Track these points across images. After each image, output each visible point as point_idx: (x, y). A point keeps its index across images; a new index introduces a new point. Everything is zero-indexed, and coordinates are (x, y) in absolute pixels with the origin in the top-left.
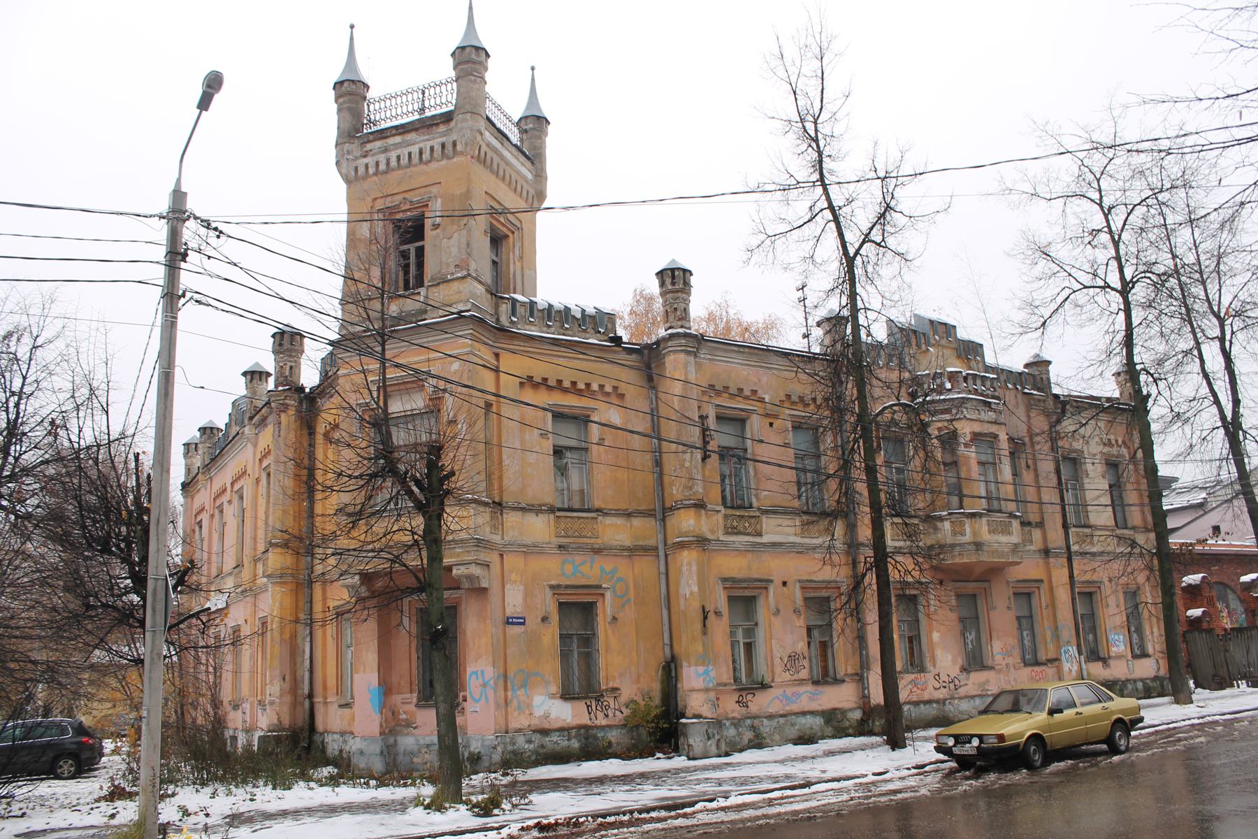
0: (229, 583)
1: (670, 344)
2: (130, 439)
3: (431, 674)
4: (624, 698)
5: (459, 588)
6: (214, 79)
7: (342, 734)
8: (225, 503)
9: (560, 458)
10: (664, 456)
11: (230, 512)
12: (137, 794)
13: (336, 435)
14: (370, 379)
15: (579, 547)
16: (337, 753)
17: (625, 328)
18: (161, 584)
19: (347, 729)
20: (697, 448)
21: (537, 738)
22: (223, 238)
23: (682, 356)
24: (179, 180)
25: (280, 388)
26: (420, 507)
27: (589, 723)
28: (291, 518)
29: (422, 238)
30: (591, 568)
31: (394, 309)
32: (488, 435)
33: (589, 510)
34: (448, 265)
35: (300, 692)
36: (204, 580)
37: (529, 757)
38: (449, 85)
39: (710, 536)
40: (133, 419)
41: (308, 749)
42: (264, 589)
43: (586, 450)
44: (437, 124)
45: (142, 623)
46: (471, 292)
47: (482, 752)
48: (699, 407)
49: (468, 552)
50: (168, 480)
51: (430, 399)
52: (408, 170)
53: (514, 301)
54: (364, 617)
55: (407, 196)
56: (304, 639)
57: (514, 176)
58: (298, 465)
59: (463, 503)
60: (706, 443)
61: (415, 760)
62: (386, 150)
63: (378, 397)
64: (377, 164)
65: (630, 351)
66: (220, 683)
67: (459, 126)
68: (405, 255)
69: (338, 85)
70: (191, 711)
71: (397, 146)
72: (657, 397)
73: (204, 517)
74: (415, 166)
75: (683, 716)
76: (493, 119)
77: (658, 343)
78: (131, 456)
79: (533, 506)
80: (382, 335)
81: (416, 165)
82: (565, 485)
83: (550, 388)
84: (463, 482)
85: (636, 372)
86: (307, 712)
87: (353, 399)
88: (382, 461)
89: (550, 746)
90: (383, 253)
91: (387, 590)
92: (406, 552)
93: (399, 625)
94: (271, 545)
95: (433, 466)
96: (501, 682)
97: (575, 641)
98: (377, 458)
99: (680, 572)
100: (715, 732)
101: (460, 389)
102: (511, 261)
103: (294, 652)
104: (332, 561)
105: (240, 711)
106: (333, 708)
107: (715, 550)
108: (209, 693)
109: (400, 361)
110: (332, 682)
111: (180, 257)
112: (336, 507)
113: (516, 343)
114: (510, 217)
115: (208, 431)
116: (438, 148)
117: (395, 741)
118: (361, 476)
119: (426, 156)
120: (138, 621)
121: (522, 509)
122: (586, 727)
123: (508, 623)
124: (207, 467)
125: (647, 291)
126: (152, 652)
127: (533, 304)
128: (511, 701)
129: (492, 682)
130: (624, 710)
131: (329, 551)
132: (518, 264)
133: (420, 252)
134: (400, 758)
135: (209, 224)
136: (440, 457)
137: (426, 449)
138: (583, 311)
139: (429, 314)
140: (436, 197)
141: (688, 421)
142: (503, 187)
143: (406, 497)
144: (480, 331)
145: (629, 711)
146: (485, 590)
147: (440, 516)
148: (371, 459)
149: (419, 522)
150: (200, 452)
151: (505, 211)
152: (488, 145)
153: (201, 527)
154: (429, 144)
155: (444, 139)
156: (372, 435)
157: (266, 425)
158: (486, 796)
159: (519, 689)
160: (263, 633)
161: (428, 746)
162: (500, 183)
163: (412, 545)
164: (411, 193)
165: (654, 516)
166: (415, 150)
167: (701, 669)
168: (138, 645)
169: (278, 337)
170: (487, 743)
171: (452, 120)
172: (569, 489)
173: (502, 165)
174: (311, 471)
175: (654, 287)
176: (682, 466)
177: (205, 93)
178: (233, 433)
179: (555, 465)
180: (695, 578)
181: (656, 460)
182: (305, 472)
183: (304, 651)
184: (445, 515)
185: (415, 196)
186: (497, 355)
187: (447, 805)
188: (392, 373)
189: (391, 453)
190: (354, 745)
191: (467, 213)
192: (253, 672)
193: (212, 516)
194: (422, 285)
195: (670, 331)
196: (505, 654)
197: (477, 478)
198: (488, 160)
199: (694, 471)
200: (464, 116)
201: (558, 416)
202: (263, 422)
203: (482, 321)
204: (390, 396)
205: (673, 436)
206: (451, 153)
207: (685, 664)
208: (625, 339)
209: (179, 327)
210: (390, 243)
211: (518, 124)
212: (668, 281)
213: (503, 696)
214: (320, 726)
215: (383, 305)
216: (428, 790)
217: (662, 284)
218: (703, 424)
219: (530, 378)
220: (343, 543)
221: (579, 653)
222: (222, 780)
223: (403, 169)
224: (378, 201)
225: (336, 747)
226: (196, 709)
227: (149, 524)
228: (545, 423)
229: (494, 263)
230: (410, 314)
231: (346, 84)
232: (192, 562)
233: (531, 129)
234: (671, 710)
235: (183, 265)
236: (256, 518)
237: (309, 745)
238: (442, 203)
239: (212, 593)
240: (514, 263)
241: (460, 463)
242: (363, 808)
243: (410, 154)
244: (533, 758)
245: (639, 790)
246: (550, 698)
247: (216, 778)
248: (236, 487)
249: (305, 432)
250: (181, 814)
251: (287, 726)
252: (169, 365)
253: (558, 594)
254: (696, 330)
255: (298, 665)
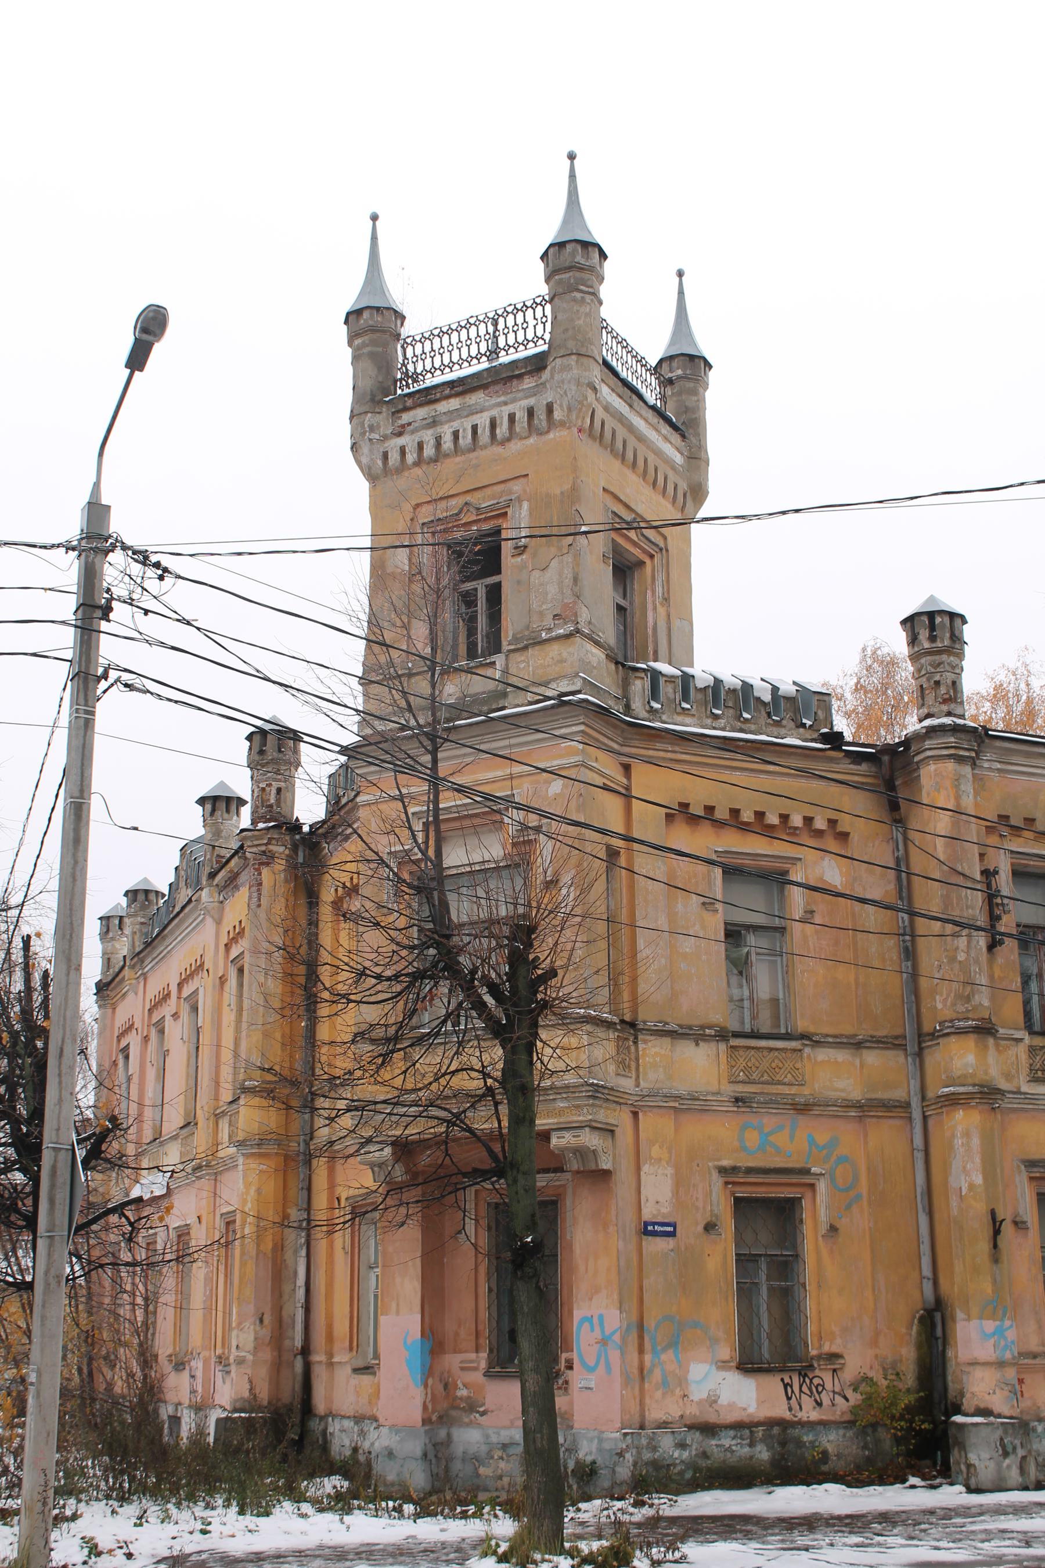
0: (172, 1156)
1: (928, 744)
2: (14, 913)
3: (513, 1319)
4: (849, 1374)
5: (559, 1170)
6: (154, 319)
7: (358, 1419)
8: (168, 1018)
9: (738, 946)
10: (921, 942)
11: (176, 1033)
12: (17, 1512)
13: (355, 905)
14: (411, 810)
15: (771, 1102)
16: (348, 1453)
17: (848, 715)
18: (64, 1158)
19: (366, 1410)
20: (979, 929)
21: (694, 1439)
22: (169, 580)
23: (950, 766)
24: (97, 486)
25: (261, 825)
26: (498, 1031)
27: (787, 1415)
28: (278, 1047)
29: (498, 571)
30: (792, 1137)
31: (451, 691)
32: (612, 907)
33: (787, 1037)
34: (541, 614)
35: (287, 1343)
36: (131, 1150)
37: (681, 1473)
38: (539, 309)
39: (1003, 1085)
40: (21, 878)
41: (299, 1444)
42: (230, 1165)
43: (782, 930)
44: (520, 377)
45: (31, 1222)
46: (581, 660)
47: (600, 1461)
48: (982, 856)
49: (577, 1107)
50: (78, 984)
51: (514, 845)
52: (472, 455)
53: (656, 675)
54: (399, 1219)
55: (468, 498)
56: (296, 1252)
57: (652, 459)
58: (291, 958)
59: (568, 1022)
60: (994, 918)
61: (482, 1470)
62: (434, 423)
63: (426, 842)
64: (420, 446)
65: (858, 758)
66: (154, 1323)
67: (557, 377)
68: (469, 600)
69: (353, 316)
70: (105, 1370)
71: (452, 415)
72: (906, 839)
73: (133, 1040)
74: (484, 447)
75: (958, 1410)
76: (614, 363)
77: (907, 743)
78: (18, 943)
79: (690, 1028)
80: (432, 737)
81: (485, 447)
82: (746, 993)
83: (719, 824)
84: (570, 988)
85: (868, 793)
86: (299, 1378)
87: (384, 845)
88: (432, 951)
89: (717, 1455)
90: (432, 597)
91: (442, 1172)
92: (473, 1106)
93: (459, 1232)
94: (245, 1090)
95: (519, 960)
96: (634, 1336)
97: (764, 1267)
98: (424, 946)
99: (951, 1147)
100: (1017, 1442)
101: (565, 828)
102: (650, 606)
103: (279, 1274)
104: (347, 1121)
105: (186, 1374)
106: (343, 1374)
107: (1014, 1110)
108: (136, 1341)
109: (459, 780)
110: (341, 1327)
111: (99, 613)
112: (354, 1029)
113: (659, 746)
114: (649, 533)
115: (141, 897)
116: (521, 416)
117: (449, 1435)
118: (396, 977)
119: (502, 430)
120: (25, 1217)
121: (672, 1034)
122: (783, 1424)
123: (646, 1233)
124: (138, 957)
125: (885, 650)
126: (47, 1273)
127: (687, 679)
128: (651, 1371)
129: (617, 1338)
130: (849, 1393)
131: (342, 1104)
132: (662, 611)
133: (495, 594)
134: (457, 1466)
135: (146, 558)
136: (531, 945)
137: (506, 930)
138: (775, 689)
139: (511, 699)
140: (519, 500)
141: (960, 880)
142: (633, 478)
143: (474, 1014)
144: (597, 726)
145: (859, 1397)
146: (606, 1174)
147: (530, 1047)
148: (414, 947)
149: (495, 1054)
150: (127, 931)
151: (637, 524)
152: (607, 408)
153: (127, 1057)
154: (506, 410)
155: (531, 401)
156: (415, 905)
157: (237, 888)
158: (605, 1543)
159: (664, 1350)
160: (228, 1244)
161: (505, 1447)
162: (628, 472)
163: (484, 1095)
164: (478, 495)
165: (902, 1047)
166: (483, 420)
167: (989, 1325)
168: (20, 1253)
169: (257, 738)
170: (607, 1446)
171: (545, 367)
172: (751, 999)
173: (632, 442)
174: (312, 968)
175: (898, 644)
176: (953, 959)
177: (137, 342)
178: (182, 899)
179: (727, 957)
180: (978, 1160)
181: (906, 949)
182: (302, 969)
183: (296, 1273)
184: (539, 1044)
185: (484, 500)
186: (627, 768)
187: (538, 1556)
188: (448, 801)
189: (448, 937)
190: (378, 1440)
191: (572, 530)
192: (209, 1309)
193: (146, 1039)
194: (498, 650)
195: (927, 722)
196: (641, 1288)
197: (592, 983)
198: (608, 434)
199: (975, 968)
200: (565, 360)
201: (733, 872)
202: (233, 882)
203: (603, 712)
204: (445, 838)
205: (935, 909)
206: (544, 424)
207: (960, 1315)
208: (848, 737)
209: (97, 729)
210: (445, 582)
211: (656, 370)
212: (924, 634)
213: (636, 1363)
214: (320, 1405)
215: (433, 686)
216: (505, 1527)
217: (913, 640)
218: (989, 886)
219: (684, 806)
220: (367, 1091)
221: (771, 1290)
222: (154, 1493)
223: (463, 453)
224: (424, 509)
225: (347, 1442)
226: (113, 1367)
227: (46, 1054)
228: (710, 884)
229: (620, 609)
230: (477, 699)
231: (366, 315)
232: (113, 1119)
233: (679, 377)
234: (936, 1395)
235: (104, 625)
236: (219, 1046)
237: (302, 1436)
238: (531, 511)
239: (144, 1173)
240: (655, 609)
241: (566, 954)
242: (392, 1555)
243: (475, 428)
244: (688, 1475)
245: (879, 1544)
246: (719, 1368)
247: (143, 1490)
248: (186, 992)
249: (302, 901)
250: (86, 1551)
251: (265, 1403)
252: (82, 791)
253: (734, 1183)
254: (974, 718)
255: (286, 1297)
